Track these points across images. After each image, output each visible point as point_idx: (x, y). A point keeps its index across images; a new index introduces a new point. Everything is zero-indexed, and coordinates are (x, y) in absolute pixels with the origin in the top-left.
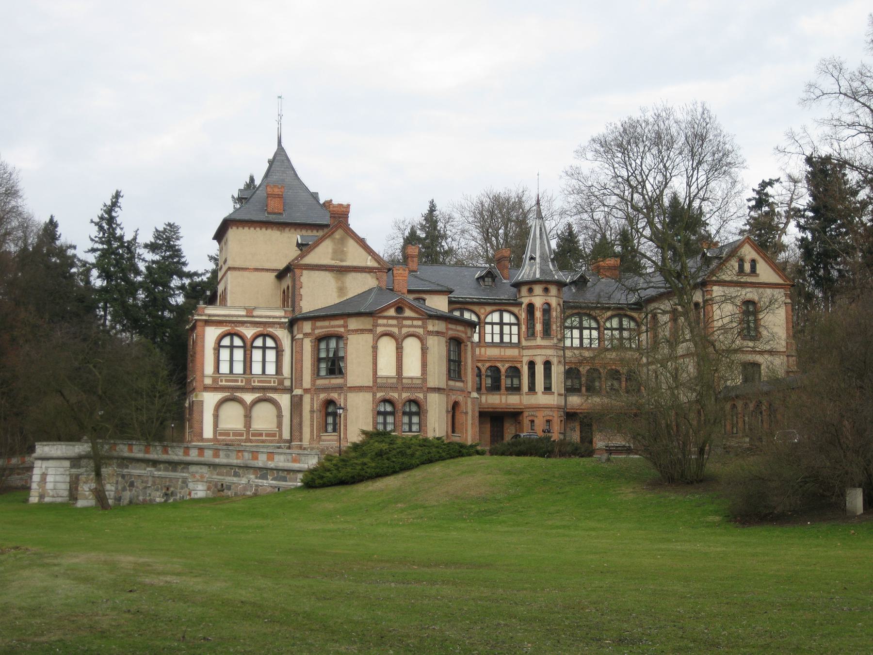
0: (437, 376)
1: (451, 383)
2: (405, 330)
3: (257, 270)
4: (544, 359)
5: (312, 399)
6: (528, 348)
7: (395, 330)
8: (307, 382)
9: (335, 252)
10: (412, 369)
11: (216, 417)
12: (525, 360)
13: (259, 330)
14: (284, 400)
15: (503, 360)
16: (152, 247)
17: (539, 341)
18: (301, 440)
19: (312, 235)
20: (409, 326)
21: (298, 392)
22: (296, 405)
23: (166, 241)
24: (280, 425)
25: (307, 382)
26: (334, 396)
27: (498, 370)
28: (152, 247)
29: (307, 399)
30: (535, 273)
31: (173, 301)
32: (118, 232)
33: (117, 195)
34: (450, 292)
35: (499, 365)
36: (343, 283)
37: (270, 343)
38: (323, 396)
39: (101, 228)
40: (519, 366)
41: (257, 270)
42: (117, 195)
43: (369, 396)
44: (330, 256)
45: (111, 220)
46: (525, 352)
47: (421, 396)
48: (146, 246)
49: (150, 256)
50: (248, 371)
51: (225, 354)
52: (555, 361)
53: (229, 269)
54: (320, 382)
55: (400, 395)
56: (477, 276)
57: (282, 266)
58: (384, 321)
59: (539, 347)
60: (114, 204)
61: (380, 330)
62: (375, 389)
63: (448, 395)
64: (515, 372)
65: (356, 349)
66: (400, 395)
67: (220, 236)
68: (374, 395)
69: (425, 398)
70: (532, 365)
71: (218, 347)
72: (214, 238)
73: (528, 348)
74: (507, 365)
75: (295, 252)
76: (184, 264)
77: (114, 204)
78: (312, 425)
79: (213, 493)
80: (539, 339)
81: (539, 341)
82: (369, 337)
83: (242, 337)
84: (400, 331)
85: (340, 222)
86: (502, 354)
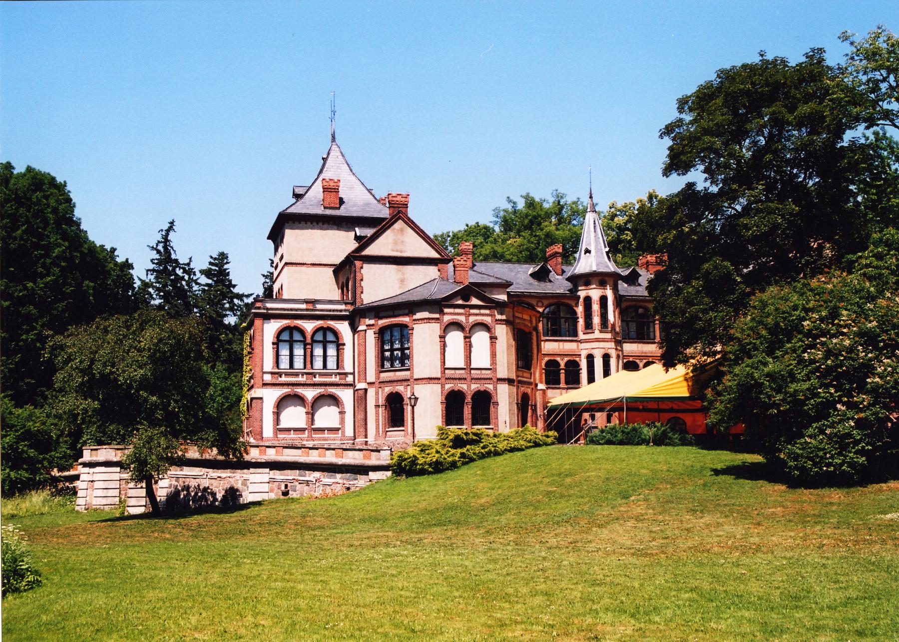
0: (506, 366)
1: (520, 374)
2: (472, 319)
3: (313, 265)
4: (602, 352)
5: (377, 393)
6: (586, 341)
7: (462, 319)
8: (371, 376)
9: (395, 243)
10: (481, 358)
11: (277, 414)
12: (584, 354)
13: (319, 323)
14: (346, 396)
15: (563, 355)
16: (207, 273)
17: (597, 334)
18: (366, 437)
19: (369, 232)
20: (477, 315)
21: (361, 386)
22: (361, 399)
23: (219, 271)
24: (342, 421)
25: (371, 376)
26: (400, 388)
27: (557, 364)
28: (207, 273)
29: (371, 392)
30: (591, 266)
31: (226, 321)
32: (173, 256)
33: (172, 223)
34: (508, 284)
35: (558, 359)
36: (403, 274)
37: (330, 337)
38: (388, 389)
39: (159, 252)
40: (577, 359)
41: (313, 265)
42: (172, 223)
43: (437, 388)
44: (390, 247)
45: (166, 240)
46: (583, 346)
47: (491, 387)
48: (202, 272)
49: (204, 280)
50: (309, 365)
51: (285, 352)
52: (613, 353)
53: (286, 264)
54: (385, 376)
55: (469, 387)
56: (530, 272)
57: (338, 259)
58: (451, 310)
59: (597, 340)
60: (171, 228)
61: (447, 318)
62: (443, 380)
63: (518, 388)
64: (573, 366)
65: (424, 336)
66: (469, 387)
67: (276, 236)
68: (443, 387)
69: (496, 389)
70: (590, 358)
71: (277, 344)
72: (268, 238)
73: (586, 341)
74: (566, 359)
75: (354, 245)
76: (234, 286)
77: (171, 228)
78: (377, 420)
79: (276, 495)
80: (597, 332)
81: (597, 334)
82: (436, 328)
83: (302, 332)
84: (467, 320)
85: (399, 212)
86: (561, 347)
